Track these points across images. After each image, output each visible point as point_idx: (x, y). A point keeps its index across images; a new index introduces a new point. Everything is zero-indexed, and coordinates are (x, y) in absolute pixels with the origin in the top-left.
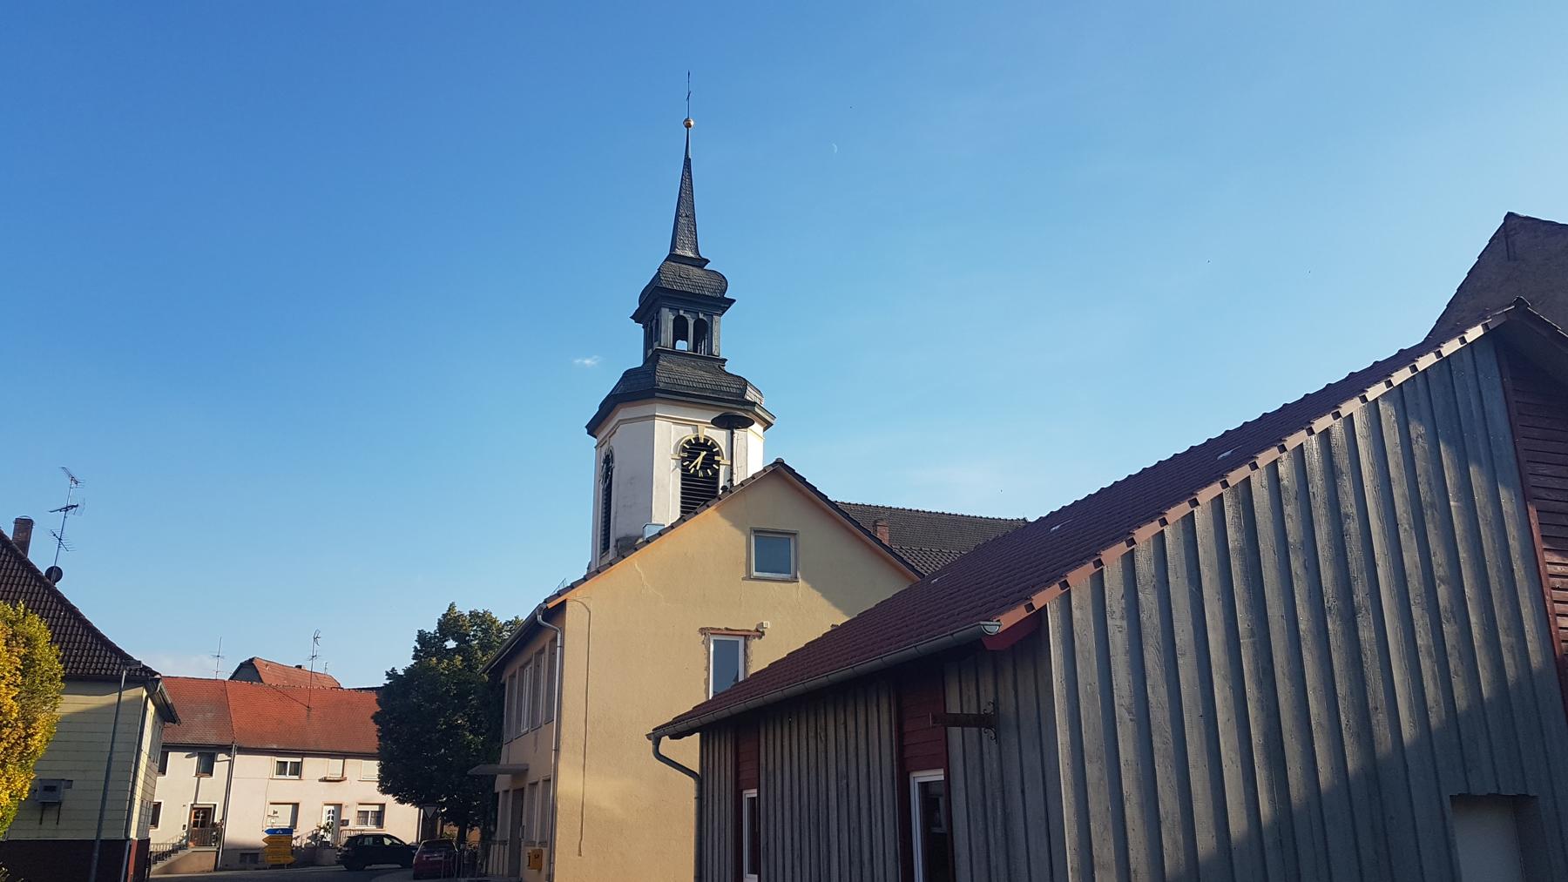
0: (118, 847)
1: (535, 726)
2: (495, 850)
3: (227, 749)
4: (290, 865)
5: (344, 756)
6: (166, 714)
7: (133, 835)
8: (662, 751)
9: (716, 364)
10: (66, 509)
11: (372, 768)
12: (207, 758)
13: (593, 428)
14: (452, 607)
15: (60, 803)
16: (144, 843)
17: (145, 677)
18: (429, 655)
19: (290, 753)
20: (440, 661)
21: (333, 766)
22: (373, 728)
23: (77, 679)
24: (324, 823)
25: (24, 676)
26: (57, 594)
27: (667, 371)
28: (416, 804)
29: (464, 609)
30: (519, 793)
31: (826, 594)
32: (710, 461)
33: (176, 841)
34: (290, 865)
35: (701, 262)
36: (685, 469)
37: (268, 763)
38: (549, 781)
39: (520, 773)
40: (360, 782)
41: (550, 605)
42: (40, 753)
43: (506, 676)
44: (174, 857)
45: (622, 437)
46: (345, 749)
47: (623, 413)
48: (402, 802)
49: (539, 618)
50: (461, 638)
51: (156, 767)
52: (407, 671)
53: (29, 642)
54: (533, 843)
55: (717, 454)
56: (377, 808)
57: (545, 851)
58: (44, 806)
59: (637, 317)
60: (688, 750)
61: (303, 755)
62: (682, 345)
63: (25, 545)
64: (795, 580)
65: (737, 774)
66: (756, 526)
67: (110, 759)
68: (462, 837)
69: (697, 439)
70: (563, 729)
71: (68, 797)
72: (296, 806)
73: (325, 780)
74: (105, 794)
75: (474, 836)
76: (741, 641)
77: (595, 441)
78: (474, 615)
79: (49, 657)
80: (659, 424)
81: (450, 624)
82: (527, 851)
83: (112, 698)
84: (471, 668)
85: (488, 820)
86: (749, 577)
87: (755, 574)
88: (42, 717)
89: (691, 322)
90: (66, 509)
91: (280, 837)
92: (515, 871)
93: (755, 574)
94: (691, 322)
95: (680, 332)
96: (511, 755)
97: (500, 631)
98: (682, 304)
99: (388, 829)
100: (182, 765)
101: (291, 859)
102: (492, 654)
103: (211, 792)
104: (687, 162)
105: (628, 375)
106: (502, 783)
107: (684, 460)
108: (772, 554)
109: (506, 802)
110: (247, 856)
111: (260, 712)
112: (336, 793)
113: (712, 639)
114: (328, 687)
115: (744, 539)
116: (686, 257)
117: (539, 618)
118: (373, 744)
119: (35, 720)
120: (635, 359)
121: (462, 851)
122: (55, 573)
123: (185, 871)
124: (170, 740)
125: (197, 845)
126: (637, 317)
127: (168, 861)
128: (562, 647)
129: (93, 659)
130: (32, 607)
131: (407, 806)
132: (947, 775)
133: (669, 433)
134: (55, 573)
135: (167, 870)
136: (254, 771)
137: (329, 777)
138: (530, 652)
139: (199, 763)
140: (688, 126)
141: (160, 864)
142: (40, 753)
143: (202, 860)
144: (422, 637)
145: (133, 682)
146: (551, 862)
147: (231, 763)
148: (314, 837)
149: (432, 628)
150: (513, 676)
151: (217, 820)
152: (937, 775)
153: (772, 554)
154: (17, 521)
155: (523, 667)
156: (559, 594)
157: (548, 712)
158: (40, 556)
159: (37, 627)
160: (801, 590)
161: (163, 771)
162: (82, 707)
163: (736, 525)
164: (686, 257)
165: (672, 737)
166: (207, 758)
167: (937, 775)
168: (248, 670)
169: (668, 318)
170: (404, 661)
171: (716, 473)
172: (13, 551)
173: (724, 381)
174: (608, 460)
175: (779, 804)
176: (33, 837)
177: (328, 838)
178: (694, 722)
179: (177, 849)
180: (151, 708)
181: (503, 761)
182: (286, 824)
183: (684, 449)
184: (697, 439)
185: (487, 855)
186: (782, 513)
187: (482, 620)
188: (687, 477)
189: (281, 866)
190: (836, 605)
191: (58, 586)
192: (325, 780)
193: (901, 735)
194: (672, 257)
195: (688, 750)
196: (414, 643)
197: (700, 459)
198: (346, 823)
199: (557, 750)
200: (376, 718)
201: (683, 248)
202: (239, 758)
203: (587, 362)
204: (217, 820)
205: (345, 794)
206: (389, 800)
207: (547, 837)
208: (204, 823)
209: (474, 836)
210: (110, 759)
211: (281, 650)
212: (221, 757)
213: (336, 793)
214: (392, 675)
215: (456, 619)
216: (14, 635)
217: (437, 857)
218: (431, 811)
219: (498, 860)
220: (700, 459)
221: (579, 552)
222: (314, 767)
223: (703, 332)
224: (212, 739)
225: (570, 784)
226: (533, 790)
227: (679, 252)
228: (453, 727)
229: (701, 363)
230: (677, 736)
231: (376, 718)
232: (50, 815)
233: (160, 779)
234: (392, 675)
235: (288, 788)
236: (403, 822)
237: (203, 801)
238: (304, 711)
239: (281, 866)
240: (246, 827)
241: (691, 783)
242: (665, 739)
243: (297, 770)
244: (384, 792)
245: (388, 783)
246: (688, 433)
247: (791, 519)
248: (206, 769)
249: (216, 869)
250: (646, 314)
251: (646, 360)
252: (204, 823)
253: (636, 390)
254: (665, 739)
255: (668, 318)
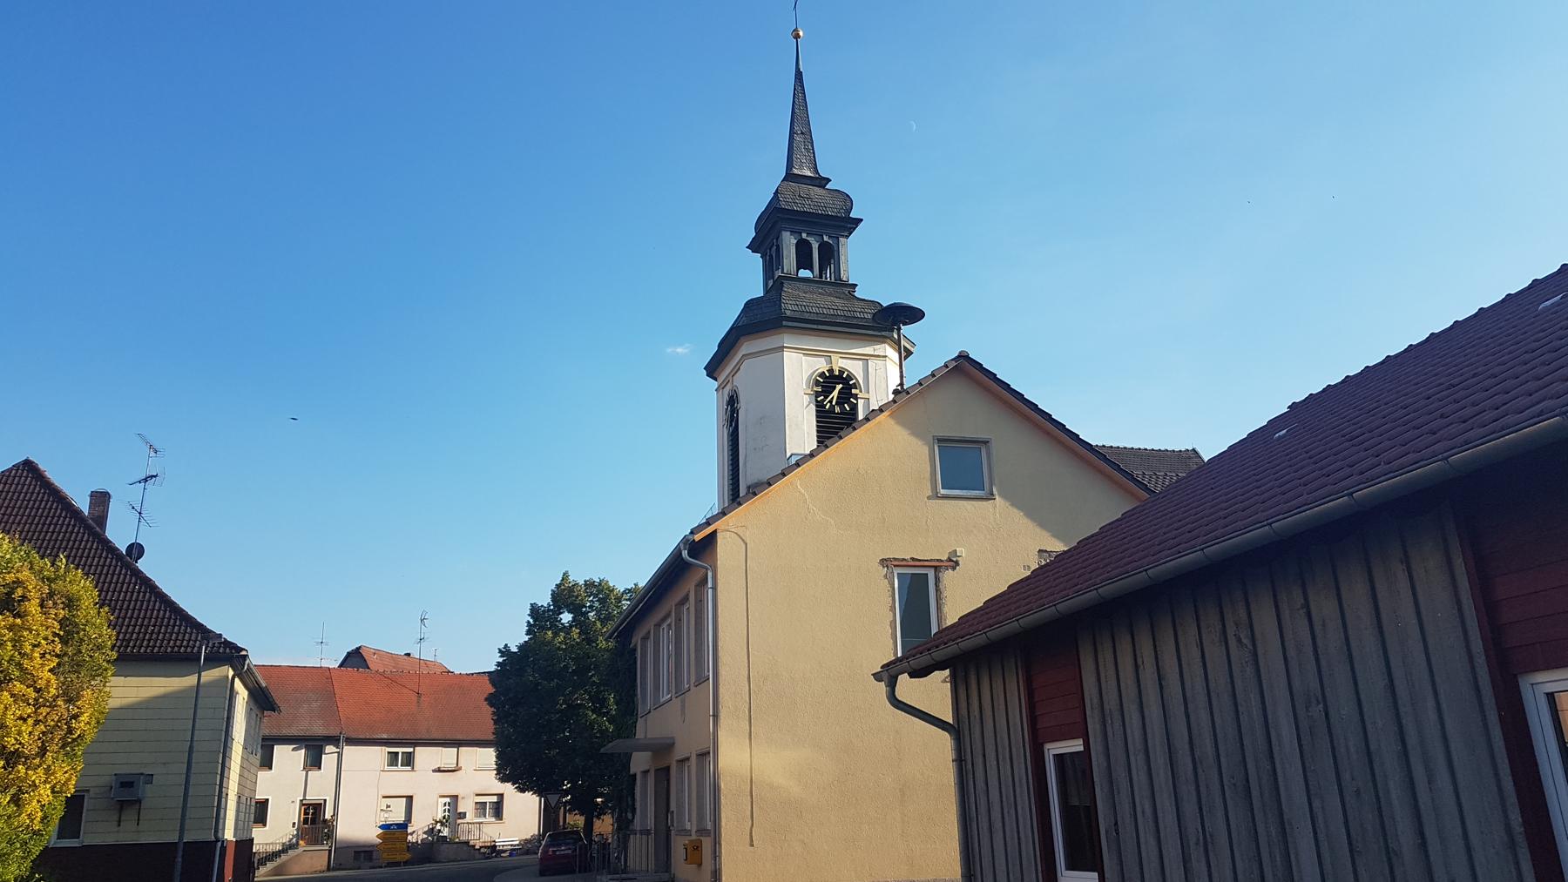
0: (206, 852)
1: (680, 693)
2: (634, 841)
3: (334, 740)
4: (406, 863)
5: (458, 744)
6: (262, 700)
7: (229, 834)
8: (900, 695)
9: (846, 290)
10: (146, 480)
11: (488, 756)
12: (314, 750)
13: (712, 369)
14: (565, 576)
15: (139, 801)
16: (245, 845)
17: (232, 655)
18: (542, 628)
19: (402, 743)
20: (556, 634)
21: (446, 756)
22: (488, 711)
23: (134, 656)
24: (440, 816)
25: (64, 642)
26: (138, 574)
27: (791, 303)
28: (540, 793)
29: (579, 577)
30: (664, 773)
31: (1032, 513)
32: (847, 395)
33: (286, 840)
34: (406, 863)
35: (822, 182)
36: (819, 405)
37: (379, 754)
38: (706, 755)
39: (663, 749)
40: (478, 769)
41: (697, 537)
42: (88, 738)
43: (637, 639)
44: (284, 857)
45: (747, 373)
46: (459, 737)
47: (746, 347)
48: (522, 790)
49: (685, 554)
50: (576, 609)
51: (256, 759)
52: (521, 647)
53: (71, 603)
54: (688, 833)
55: (855, 386)
56: (495, 799)
57: (707, 844)
58: (122, 806)
59: (754, 246)
60: (934, 692)
61: (415, 744)
62: (804, 273)
63: (101, 520)
64: (990, 497)
65: (1033, 721)
66: (941, 434)
67: (191, 747)
68: (589, 825)
69: (831, 371)
70: (722, 690)
71: (149, 793)
72: (410, 799)
73: (439, 770)
74: (186, 789)
75: (605, 826)
76: (931, 574)
77: (715, 384)
78: (589, 584)
79: (98, 627)
80: (788, 356)
81: (565, 596)
82: (679, 845)
83: (191, 680)
84: (589, 641)
85: (623, 805)
86: (936, 496)
87: (943, 492)
88: (87, 693)
89: (815, 246)
90: (146, 480)
91: (394, 832)
92: (665, 863)
93: (943, 492)
94: (815, 246)
95: (804, 260)
96: (649, 728)
97: (619, 600)
98: (804, 228)
99: (492, 784)
100: (288, 758)
101: (408, 856)
102: (610, 626)
103: (320, 786)
104: (799, 75)
105: (750, 305)
106: (640, 762)
107: (817, 394)
108: (961, 468)
109: (645, 786)
110: (361, 854)
111: (365, 703)
112: (451, 784)
113: (896, 571)
114: (439, 671)
115: (926, 450)
116: (802, 175)
117: (685, 554)
118: (487, 728)
119: (78, 697)
120: (754, 286)
121: (591, 841)
122: (136, 550)
123: (297, 871)
124: (275, 732)
125: (309, 843)
126: (754, 246)
127: (278, 861)
128: (714, 588)
129: (159, 632)
130: (76, 560)
131: (528, 795)
132: (1087, 744)
133: (799, 365)
134: (136, 550)
135: (278, 871)
136: (363, 762)
137: (443, 766)
138: (670, 603)
139: (306, 756)
140: (797, 37)
141: (270, 865)
142: (88, 738)
143: (314, 859)
144: (535, 611)
145: (215, 660)
146: (716, 855)
147: (340, 755)
148: (431, 831)
149: (545, 600)
150: (645, 638)
151: (328, 816)
152: (1076, 746)
153: (961, 468)
154: (94, 495)
155: (658, 625)
156: (708, 523)
157: (699, 670)
158: (119, 533)
159: (83, 587)
160: (997, 510)
161: (267, 763)
162: (161, 691)
163: (916, 432)
164: (802, 175)
165: (914, 674)
166: (314, 750)
167: (1076, 746)
168: (355, 658)
169: (789, 242)
170: (517, 637)
171: (854, 407)
172: (88, 527)
173: (858, 306)
174: (733, 401)
175: (1137, 761)
176: (110, 840)
177: (445, 832)
178: (938, 655)
179: (287, 848)
180: (242, 693)
181: (640, 734)
182: (401, 819)
183: (817, 383)
184: (831, 371)
185: (626, 849)
186: (971, 417)
187: (599, 590)
188: (822, 413)
189: (397, 864)
190: (1043, 524)
191: (142, 565)
192: (439, 770)
193: (1489, 609)
194: (790, 177)
195: (934, 692)
196: (525, 617)
197: (835, 393)
198: (463, 815)
199: (716, 716)
200: (491, 700)
201: (801, 168)
202: (349, 751)
203: (679, 350)
204: (328, 816)
205: (467, 790)
206: (508, 789)
207: (709, 826)
208: (315, 821)
209: (605, 826)
210: (191, 747)
211: (389, 638)
212: (329, 748)
213: (451, 784)
214: (505, 652)
215: (571, 589)
216: (51, 595)
217: (564, 850)
218: (553, 799)
219: (640, 853)
220: (835, 393)
221: (706, 495)
222: (427, 757)
223: (830, 255)
224: (319, 730)
225: (733, 757)
226: (684, 773)
227: (796, 171)
228: (573, 708)
229: (829, 289)
230: (919, 673)
231: (491, 700)
232: (130, 815)
233: (263, 775)
234: (505, 652)
235: (401, 780)
236: (522, 817)
237: (313, 796)
238: (415, 698)
239: (397, 864)
240: (358, 823)
241: (945, 740)
242: (904, 678)
243: (409, 760)
244: (503, 780)
245: (507, 771)
246: (821, 365)
247: (983, 423)
248: (314, 762)
249: (329, 869)
250: (765, 241)
251: (767, 290)
252: (315, 821)
253: (761, 321)
254: (904, 678)
255: (789, 242)
